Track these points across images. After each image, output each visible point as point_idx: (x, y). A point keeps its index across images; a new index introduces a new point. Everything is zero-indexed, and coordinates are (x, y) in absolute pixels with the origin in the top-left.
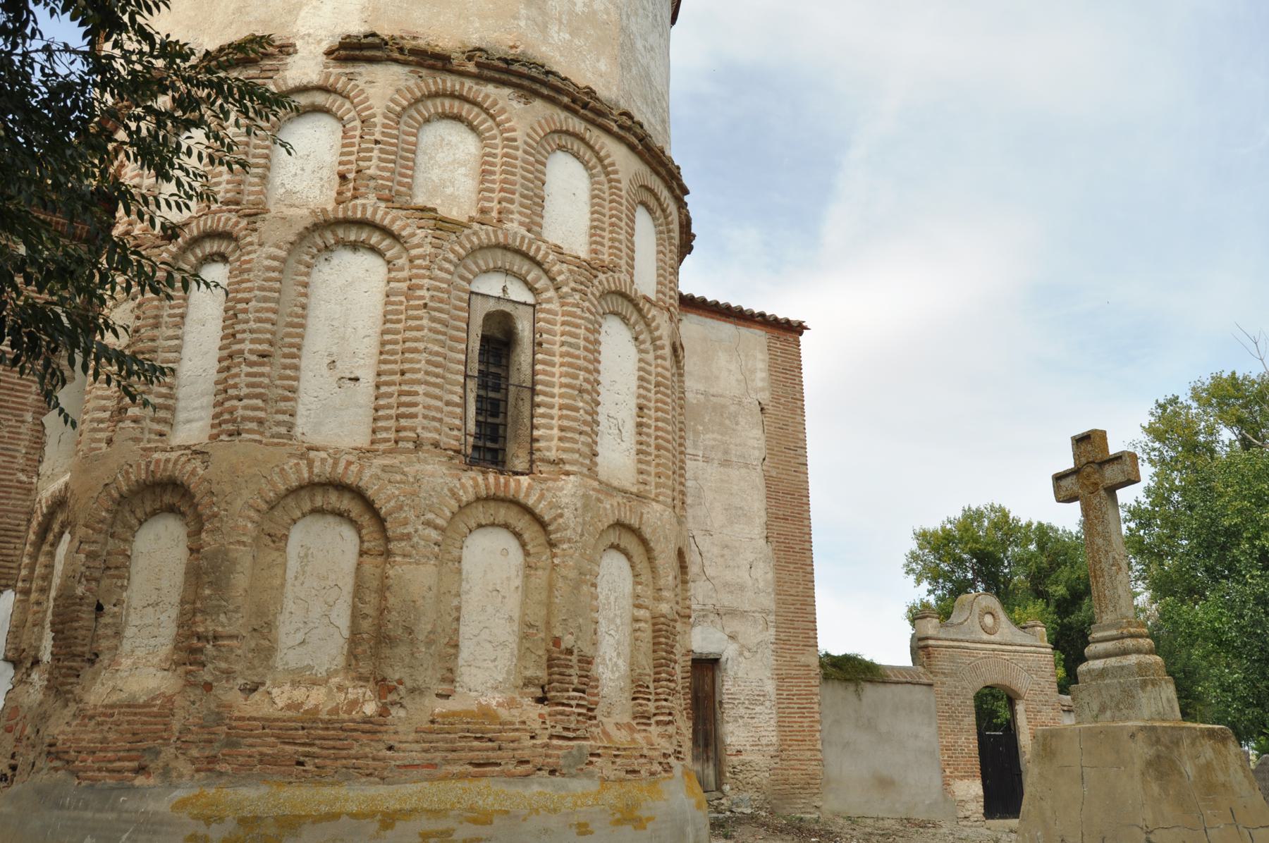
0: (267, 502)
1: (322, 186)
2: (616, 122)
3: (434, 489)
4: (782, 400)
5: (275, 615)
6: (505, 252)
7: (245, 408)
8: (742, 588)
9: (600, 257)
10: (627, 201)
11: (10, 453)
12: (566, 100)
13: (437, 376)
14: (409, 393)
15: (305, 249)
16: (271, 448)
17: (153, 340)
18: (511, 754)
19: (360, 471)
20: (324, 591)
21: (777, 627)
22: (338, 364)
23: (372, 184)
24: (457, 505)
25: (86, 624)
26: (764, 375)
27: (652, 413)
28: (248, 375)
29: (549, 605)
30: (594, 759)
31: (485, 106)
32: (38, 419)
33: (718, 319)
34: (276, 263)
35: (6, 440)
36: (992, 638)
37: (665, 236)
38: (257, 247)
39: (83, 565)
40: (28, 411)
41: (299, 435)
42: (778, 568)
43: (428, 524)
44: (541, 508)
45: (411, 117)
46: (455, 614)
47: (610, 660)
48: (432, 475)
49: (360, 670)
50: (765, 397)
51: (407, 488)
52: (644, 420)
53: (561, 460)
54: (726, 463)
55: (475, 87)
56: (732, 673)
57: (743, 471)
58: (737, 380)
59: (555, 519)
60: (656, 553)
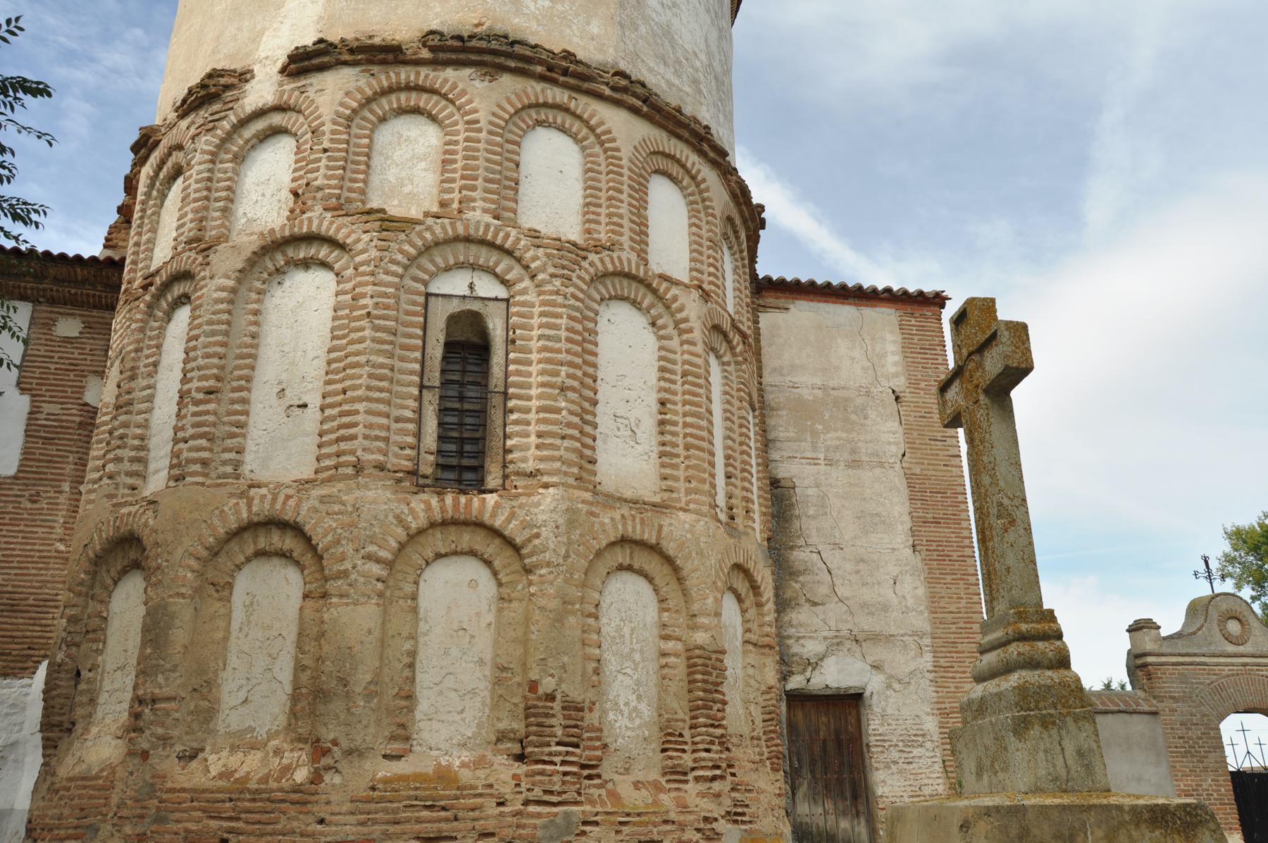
0: (207, 549)
1: (280, 208)
2: (607, 84)
3: (375, 518)
4: (923, 385)
5: (216, 673)
6: (468, 245)
7: (190, 450)
8: (885, 608)
9: (595, 236)
10: (630, 170)
11: (48, 524)
12: (539, 69)
13: (381, 390)
14: (348, 413)
15: (256, 276)
16: (212, 490)
17: (129, 393)
18: (470, 825)
19: (298, 505)
20: (269, 642)
21: (935, 652)
22: (287, 392)
23: (319, 195)
24: (405, 533)
25: (64, 692)
26: (897, 358)
27: (679, 408)
28: (194, 414)
29: (525, 642)
30: (588, 828)
31: (443, 91)
32: (76, 488)
33: (833, 302)
34: (224, 294)
35: (45, 512)
36: (1241, 649)
37: (700, 206)
38: (208, 280)
39: (65, 630)
40: (65, 481)
41: (247, 472)
42: (931, 581)
43: (369, 557)
44: (511, 529)
45: (363, 119)
46: (406, 660)
47: (626, 704)
48: (374, 502)
49: (299, 730)
50: (900, 383)
51: (346, 519)
52: (668, 417)
53: (538, 470)
54: (855, 464)
55: (432, 74)
56: (879, 710)
57: (878, 471)
58: (863, 368)
59: (529, 540)
60: (684, 573)
